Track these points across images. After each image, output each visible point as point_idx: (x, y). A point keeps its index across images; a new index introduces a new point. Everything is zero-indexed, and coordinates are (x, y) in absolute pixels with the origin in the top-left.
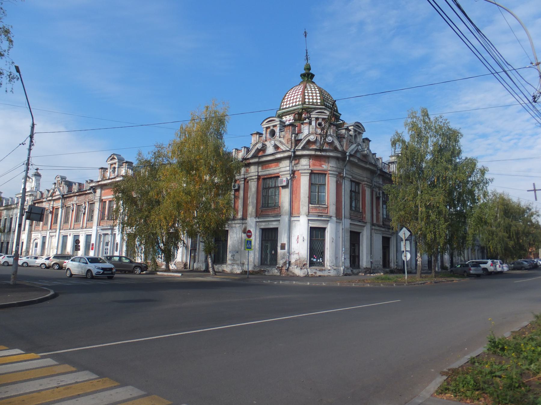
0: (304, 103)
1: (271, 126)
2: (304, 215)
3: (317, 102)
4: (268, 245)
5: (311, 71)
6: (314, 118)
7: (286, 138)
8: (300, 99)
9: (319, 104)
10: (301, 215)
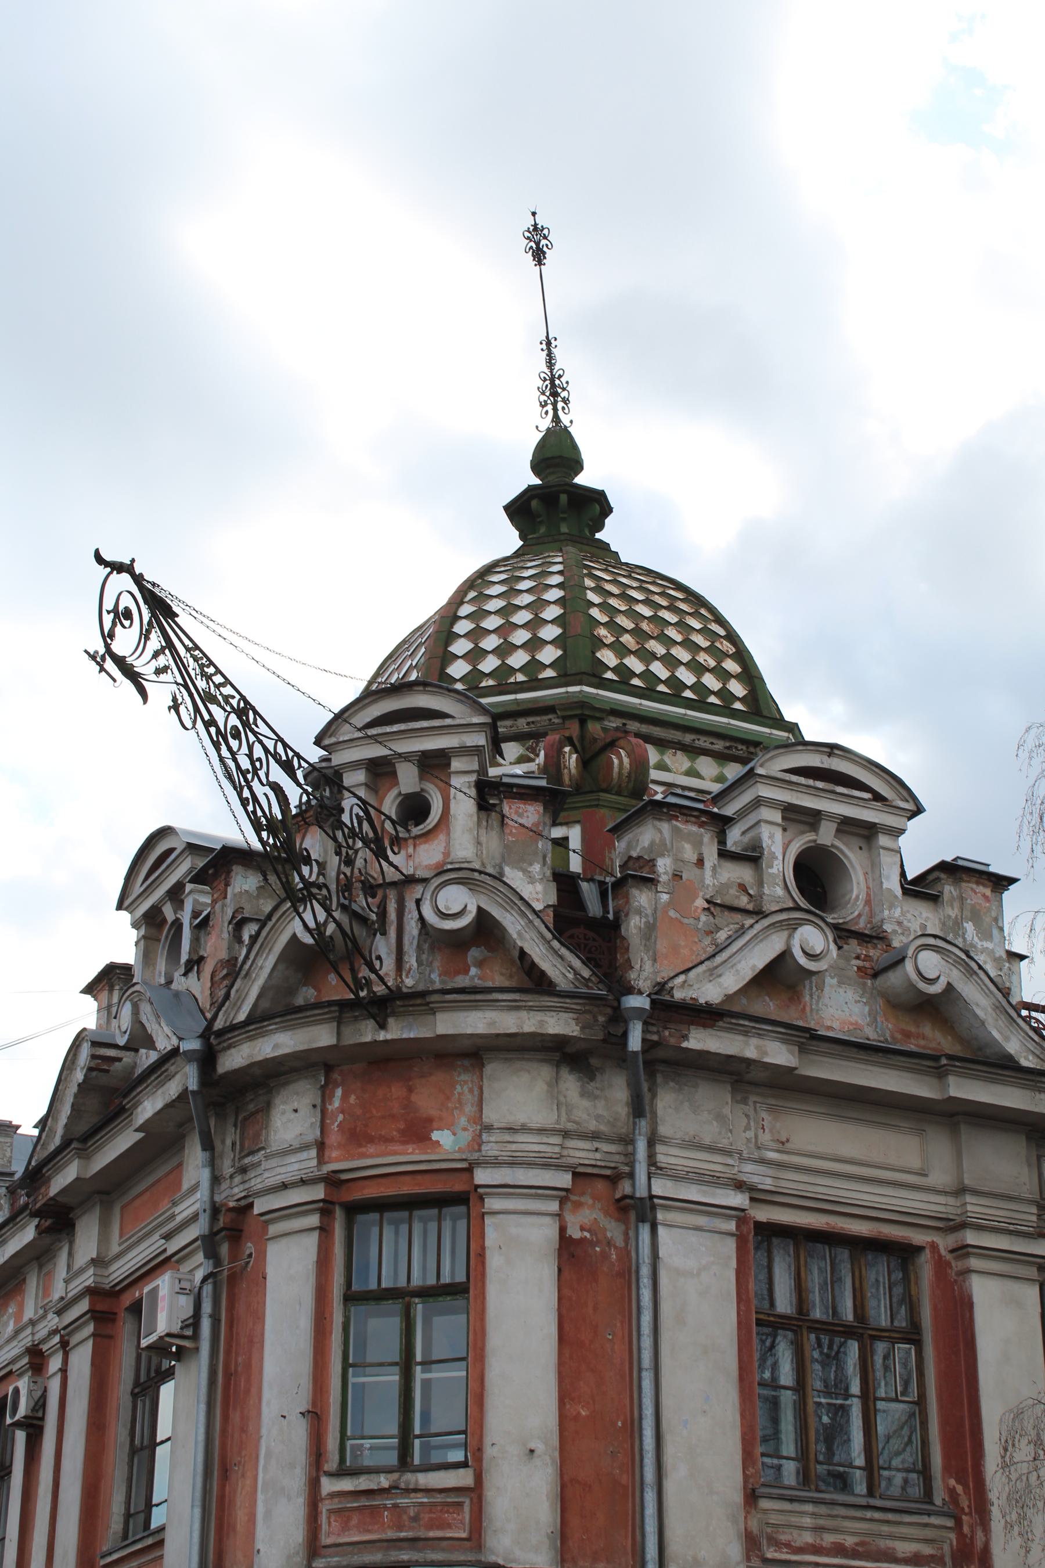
6: (355, 765)
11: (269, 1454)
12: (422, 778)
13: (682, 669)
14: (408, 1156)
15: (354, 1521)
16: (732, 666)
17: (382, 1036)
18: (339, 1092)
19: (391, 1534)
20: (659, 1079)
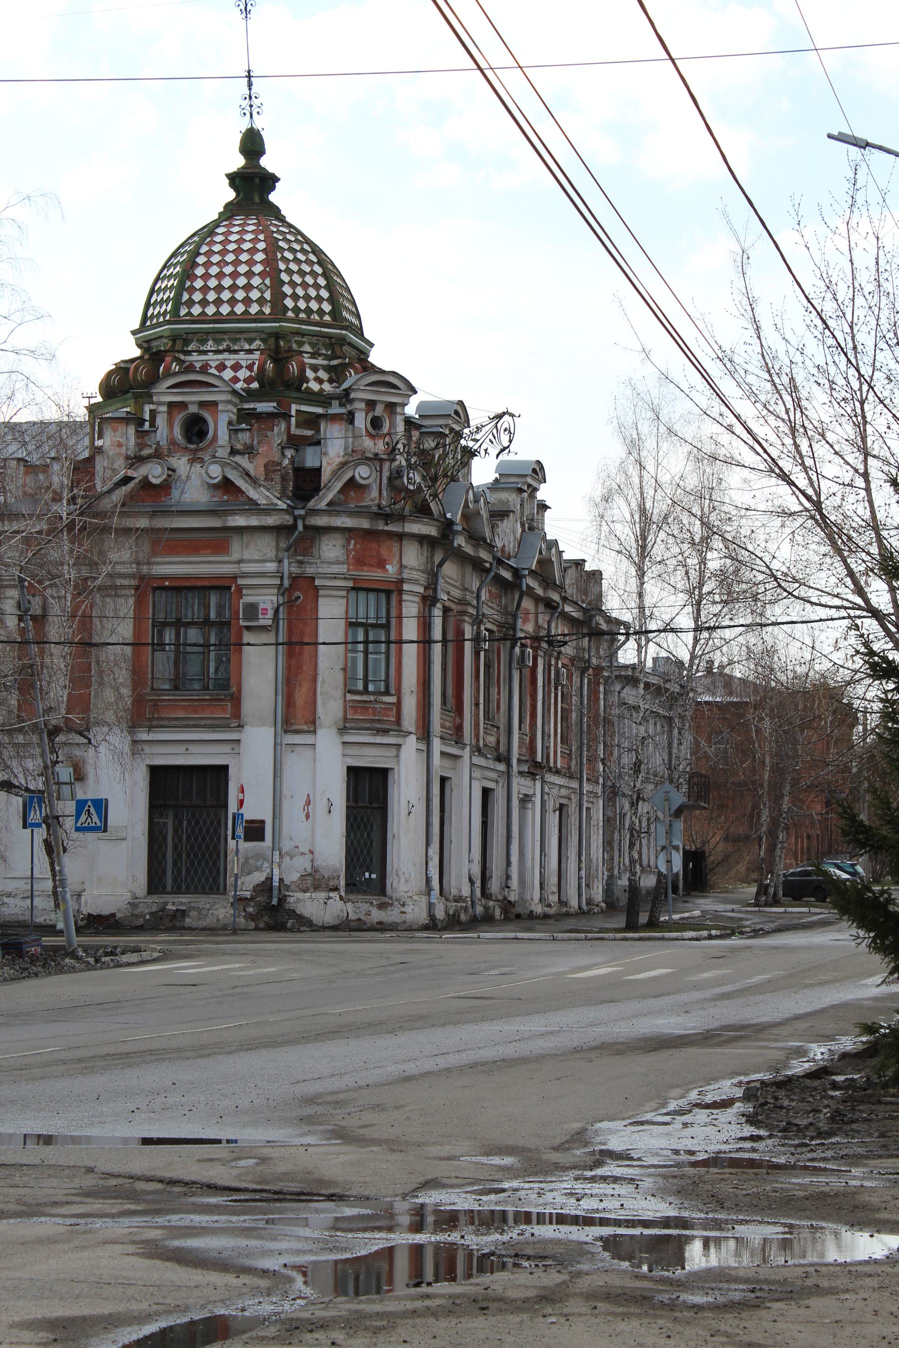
0: (279, 309)
1: (193, 403)
2: (328, 727)
3: (321, 312)
4: (165, 824)
5: (264, 162)
6: (362, 400)
7: (261, 461)
8: (262, 292)
9: (327, 318)
10: (321, 727)
11: (323, 682)
12: (384, 411)
13: (291, 263)
14: (377, 574)
15: (359, 711)
16: (318, 269)
17: (386, 528)
18: (353, 542)
19: (372, 717)
20: (404, 542)
